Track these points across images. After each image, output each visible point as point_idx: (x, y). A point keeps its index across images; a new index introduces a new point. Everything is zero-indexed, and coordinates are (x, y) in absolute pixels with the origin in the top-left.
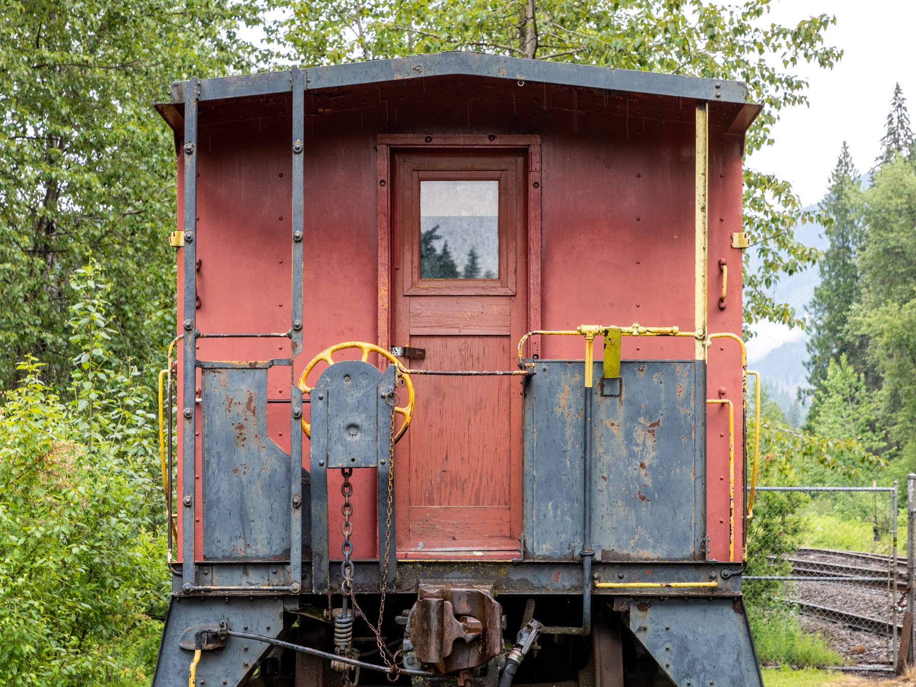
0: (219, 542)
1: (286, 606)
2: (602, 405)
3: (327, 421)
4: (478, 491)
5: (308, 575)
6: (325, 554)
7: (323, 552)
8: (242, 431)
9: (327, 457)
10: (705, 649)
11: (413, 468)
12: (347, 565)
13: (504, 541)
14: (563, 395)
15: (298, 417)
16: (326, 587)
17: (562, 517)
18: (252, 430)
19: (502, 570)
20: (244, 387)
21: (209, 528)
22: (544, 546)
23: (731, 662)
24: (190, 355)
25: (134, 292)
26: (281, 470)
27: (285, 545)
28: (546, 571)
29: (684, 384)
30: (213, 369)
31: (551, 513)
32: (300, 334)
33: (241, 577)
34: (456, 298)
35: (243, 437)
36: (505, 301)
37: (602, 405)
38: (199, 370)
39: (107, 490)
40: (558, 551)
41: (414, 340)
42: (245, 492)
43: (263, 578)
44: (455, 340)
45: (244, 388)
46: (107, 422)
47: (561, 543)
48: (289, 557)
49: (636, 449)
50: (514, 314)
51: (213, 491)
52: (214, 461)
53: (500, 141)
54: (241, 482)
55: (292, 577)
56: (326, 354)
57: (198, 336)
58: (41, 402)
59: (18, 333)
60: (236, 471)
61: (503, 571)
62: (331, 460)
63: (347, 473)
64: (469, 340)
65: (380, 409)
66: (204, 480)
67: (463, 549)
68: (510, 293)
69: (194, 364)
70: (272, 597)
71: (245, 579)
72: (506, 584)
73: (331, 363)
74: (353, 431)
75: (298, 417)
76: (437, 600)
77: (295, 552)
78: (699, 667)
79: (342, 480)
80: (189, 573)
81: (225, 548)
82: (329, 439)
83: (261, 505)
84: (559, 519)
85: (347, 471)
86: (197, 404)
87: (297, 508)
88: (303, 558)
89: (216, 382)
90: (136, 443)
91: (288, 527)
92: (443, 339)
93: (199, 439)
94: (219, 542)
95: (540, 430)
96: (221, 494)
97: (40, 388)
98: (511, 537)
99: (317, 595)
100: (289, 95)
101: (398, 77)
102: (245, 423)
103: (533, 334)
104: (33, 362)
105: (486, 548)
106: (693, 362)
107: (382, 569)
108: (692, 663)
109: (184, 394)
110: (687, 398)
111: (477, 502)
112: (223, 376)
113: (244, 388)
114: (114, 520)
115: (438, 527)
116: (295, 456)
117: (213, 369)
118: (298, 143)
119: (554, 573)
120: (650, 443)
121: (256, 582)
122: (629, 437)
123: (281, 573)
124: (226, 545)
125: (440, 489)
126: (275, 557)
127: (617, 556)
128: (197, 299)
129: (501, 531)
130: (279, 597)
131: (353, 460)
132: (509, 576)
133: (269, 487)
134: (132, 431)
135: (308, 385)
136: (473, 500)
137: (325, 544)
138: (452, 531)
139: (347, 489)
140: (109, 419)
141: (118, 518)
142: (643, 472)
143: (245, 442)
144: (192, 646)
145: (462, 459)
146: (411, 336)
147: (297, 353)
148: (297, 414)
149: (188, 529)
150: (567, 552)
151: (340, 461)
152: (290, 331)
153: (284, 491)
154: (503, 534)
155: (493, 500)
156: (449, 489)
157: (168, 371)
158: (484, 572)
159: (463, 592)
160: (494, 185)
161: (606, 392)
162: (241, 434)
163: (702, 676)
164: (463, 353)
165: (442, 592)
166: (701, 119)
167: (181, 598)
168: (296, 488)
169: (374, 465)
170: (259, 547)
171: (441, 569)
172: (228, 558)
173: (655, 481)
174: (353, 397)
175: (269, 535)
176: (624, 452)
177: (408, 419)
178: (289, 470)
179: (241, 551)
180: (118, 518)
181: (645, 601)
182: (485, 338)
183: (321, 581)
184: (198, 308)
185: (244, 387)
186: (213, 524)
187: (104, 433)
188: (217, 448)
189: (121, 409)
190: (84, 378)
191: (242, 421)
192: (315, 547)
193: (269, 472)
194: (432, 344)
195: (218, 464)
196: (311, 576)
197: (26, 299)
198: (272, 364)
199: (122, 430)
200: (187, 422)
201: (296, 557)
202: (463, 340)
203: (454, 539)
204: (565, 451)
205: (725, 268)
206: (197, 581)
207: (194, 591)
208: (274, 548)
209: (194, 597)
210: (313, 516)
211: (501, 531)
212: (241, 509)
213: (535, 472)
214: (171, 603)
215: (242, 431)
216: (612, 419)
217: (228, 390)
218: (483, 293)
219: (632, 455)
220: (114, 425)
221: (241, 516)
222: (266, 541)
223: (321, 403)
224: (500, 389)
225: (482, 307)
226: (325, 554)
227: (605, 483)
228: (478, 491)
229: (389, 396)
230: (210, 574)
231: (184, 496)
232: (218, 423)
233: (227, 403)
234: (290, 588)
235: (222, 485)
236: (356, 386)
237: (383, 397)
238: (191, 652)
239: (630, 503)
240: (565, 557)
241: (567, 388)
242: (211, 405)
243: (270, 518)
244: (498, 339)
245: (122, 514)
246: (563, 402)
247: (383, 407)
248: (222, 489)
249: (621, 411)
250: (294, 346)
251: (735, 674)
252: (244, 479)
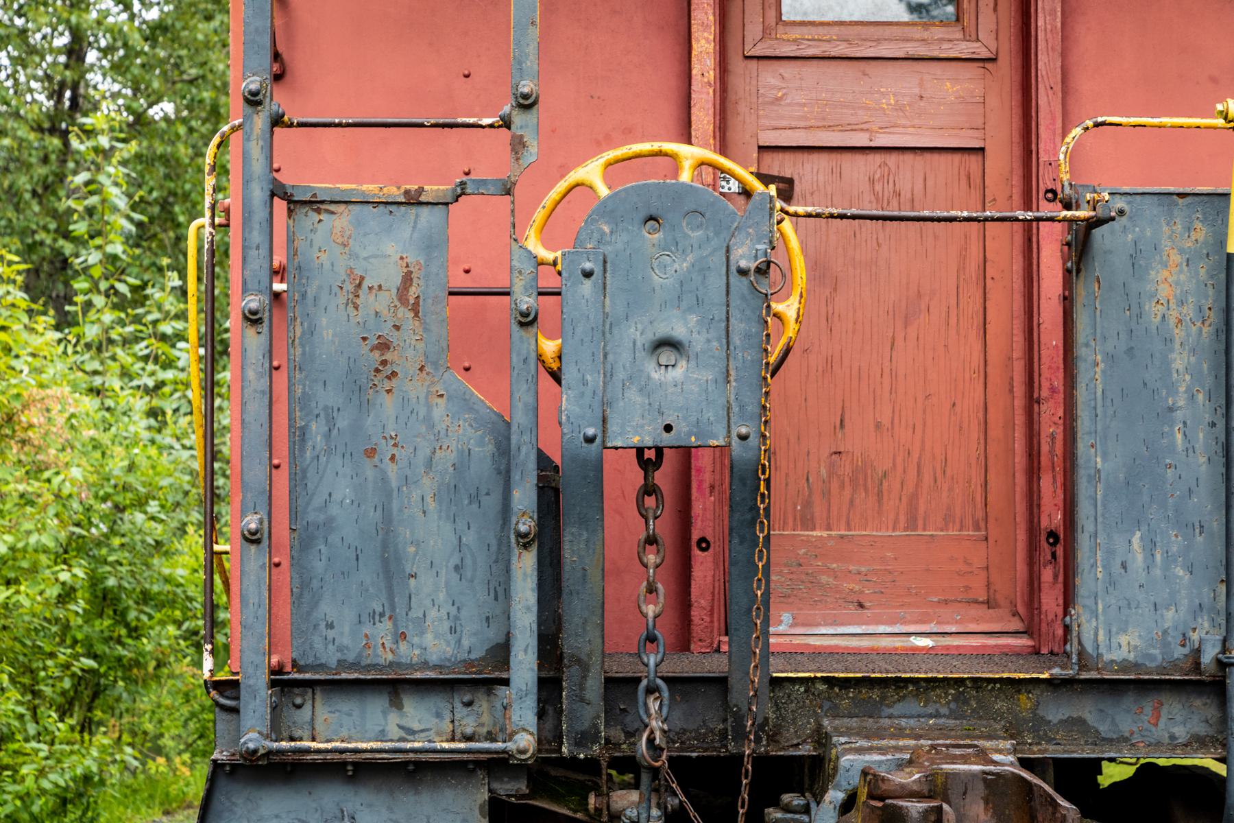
0: (330, 626)
1: (496, 786)
3: (606, 328)
4: (914, 498)
5: (550, 710)
6: (596, 660)
7: (589, 655)
8: (388, 356)
9: (604, 421)
12: (650, 690)
13: (974, 611)
14: (1166, 274)
15: (528, 321)
16: (595, 738)
17: (1166, 568)
18: (410, 353)
19: (1023, 697)
20: (392, 249)
21: (305, 592)
22: (1124, 639)
24: (258, 165)
25: (188, 187)
26: (484, 451)
27: (493, 635)
28: (1129, 701)
30: (315, 204)
31: (1140, 557)
32: (530, 118)
33: (385, 714)
34: (862, 64)
35: (388, 370)
36: (973, 70)
38: (280, 206)
39: (131, 468)
40: (1156, 652)
41: (768, 157)
42: (395, 505)
43: (438, 715)
44: (860, 159)
45: (389, 250)
46: (130, 360)
47: (1165, 632)
48: (505, 663)
50: (993, 102)
51: (318, 501)
52: (317, 429)
54: (384, 479)
55: (515, 718)
56: (591, 172)
57: (277, 121)
58: (25, 326)
59: (22, 242)
60: (371, 453)
61: (1025, 701)
62: (613, 428)
63: (648, 459)
64: (892, 159)
65: (735, 301)
66: (293, 477)
67: (882, 629)
68: (984, 54)
69: (268, 187)
70: (463, 763)
72: (1034, 730)
73: (603, 191)
74: (667, 356)
75: (528, 321)
76: (922, 806)
77: (521, 656)
79: (636, 476)
80: (257, 701)
81: (346, 641)
82: (608, 376)
83: (434, 538)
84: (1157, 572)
85: (650, 454)
86: (277, 296)
87: (526, 546)
88: (541, 667)
89: (325, 236)
90: (177, 395)
91: (502, 591)
92: (835, 156)
93: (281, 379)
94: (330, 626)
95: (1111, 358)
96: (334, 510)
97: (24, 305)
98: (989, 604)
99: (574, 759)
102: (394, 337)
103: (1097, 125)
104: (10, 263)
105: (933, 627)
107: (736, 697)
109: (244, 259)
111: (912, 524)
112: (341, 220)
113: (389, 250)
114: (139, 517)
115: (824, 579)
116: (520, 418)
117: (315, 204)
119: (1148, 706)
121: (423, 728)
123: (482, 704)
124: (346, 633)
125: (827, 494)
126: (469, 664)
128: (276, 56)
129: (967, 588)
130: (478, 763)
131: (668, 428)
132: (1041, 712)
133: (456, 492)
134: (169, 375)
135: (547, 246)
136: (902, 518)
137: (593, 634)
138: (857, 588)
139: (650, 501)
140: (134, 355)
141: (146, 513)
143: (395, 383)
145: (878, 426)
146: (762, 149)
147: (525, 162)
148: (525, 314)
149: (253, 599)
150: (1179, 652)
151: (635, 429)
152: (507, 109)
153: (492, 502)
154: (971, 596)
155: (947, 521)
156: (848, 492)
157: (205, 220)
158: (979, 701)
159: (973, 775)
162: (384, 363)
164: (878, 187)
165: (930, 778)
167: (235, 768)
168: (524, 497)
169: (721, 442)
170: (429, 638)
171: (875, 695)
172: (354, 666)
174: (668, 272)
175: (453, 611)
177: (791, 330)
178: (504, 450)
179: (383, 648)
180: (146, 513)
182: (928, 156)
183: (585, 725)
184: (278, 78)
185: (392, 249)
186: (315, 584)
187: (125, 374)
188: (329, 397)
189: (153, 340)
190: (95, 288)
191: (386, 330)
192: (570, 643)
193: (452, 457)
194: (808, 166)
195: (328, 435)
196: (560, 712)
197: (34, 193)
198: (461, 192)
199: (153, 374)
200: (251, 332)
201: (524, 666)
202: (878, 158)
203: (861, 606)
204: (1171, 410)
205: (1100, 119)
206: (276, 728)
207: (270, 753)
208: (466, 643)
209: (271, 766)
210: (567, 568)
211: (967, 588)
212: (385, 546)
214: (212, 781)
215: (388, 356)
217: (354, 256)
218: (923, 51)
220: (141, 364)
221: (385, 563)
222: (446, 625)
223: (588, 284)
224: (961, 269)
225: (921, 85)
226: (596, 660)
228: (914, 498)
229: (759, 270)
230: (308, 706)
231: (243, 514)
232: (328, 334)
233: (349, 287)
234: (510, 746)
235: (338, 489)
236: (674, 246)
237: (743, 272)
240: (1175, 665)
241: (1176, 258)
242: (311, 291)
243: (457, 568)
244: (957, 157)
245: (153, 507)
247: (743, 298)
248: (337, 496)
250: (518, 145)
252: (392, 471)
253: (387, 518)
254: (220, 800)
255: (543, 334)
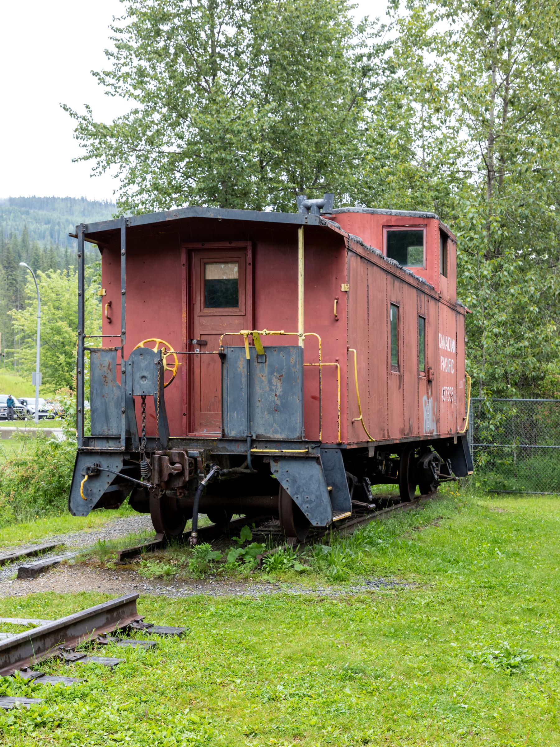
2: (257, 367)
10: (304, 481)
11: (202, 395)
23: (316, 488)
28: (233, 444)
29: (294, 357)
37: (257, 367)
41: (202, 336)
49: (273, 388)
53: (234, 245)
61: (215, 443)
63: (144, 398)
71: (107, 445)
74: (144, 379)
78: (301, 490)
83: (113, 411)
100: (119, 230)
101: (168, 219)
106: (298, 347)
108: (298, 488)
110: (295, 364)
118: (123, 251)
119: (237, 445)
120: (279, 385)
121: (111, 446)
122: (270, 382)
127: (265, 437)
142: (276, 398)
144: (84, 474)
151: (138, 393)
160: (237, 265)
161: (259, 361)
163: (303, 494)
166: (301, 233)
173: (282, 402)
174: (143, 364)
176: (268, 389)
181: (277, 458)
201: (123, 436)
213: (229, 399)
216: (262, 374)
219: (271, 390)
227: (259, 403)
238: (84, 476)
239: (270, 412)
246: (241, 366)
249: (266, 370)
251: (318, 493)
252: (107, 400)
253: (106, 409)
254: (79, 459)
255: (443, 334)
